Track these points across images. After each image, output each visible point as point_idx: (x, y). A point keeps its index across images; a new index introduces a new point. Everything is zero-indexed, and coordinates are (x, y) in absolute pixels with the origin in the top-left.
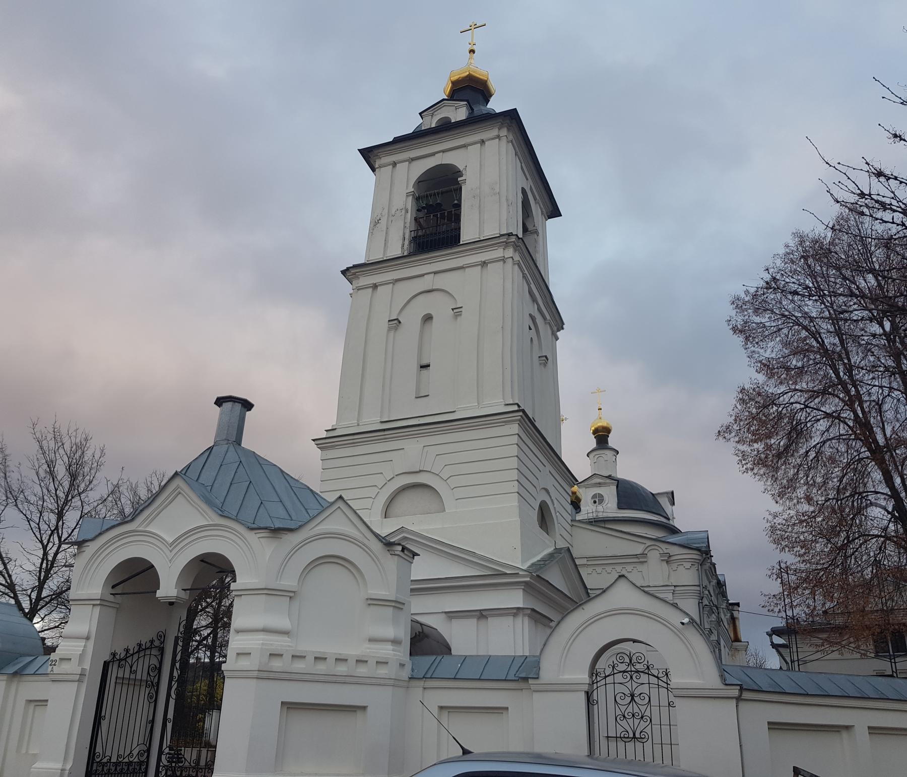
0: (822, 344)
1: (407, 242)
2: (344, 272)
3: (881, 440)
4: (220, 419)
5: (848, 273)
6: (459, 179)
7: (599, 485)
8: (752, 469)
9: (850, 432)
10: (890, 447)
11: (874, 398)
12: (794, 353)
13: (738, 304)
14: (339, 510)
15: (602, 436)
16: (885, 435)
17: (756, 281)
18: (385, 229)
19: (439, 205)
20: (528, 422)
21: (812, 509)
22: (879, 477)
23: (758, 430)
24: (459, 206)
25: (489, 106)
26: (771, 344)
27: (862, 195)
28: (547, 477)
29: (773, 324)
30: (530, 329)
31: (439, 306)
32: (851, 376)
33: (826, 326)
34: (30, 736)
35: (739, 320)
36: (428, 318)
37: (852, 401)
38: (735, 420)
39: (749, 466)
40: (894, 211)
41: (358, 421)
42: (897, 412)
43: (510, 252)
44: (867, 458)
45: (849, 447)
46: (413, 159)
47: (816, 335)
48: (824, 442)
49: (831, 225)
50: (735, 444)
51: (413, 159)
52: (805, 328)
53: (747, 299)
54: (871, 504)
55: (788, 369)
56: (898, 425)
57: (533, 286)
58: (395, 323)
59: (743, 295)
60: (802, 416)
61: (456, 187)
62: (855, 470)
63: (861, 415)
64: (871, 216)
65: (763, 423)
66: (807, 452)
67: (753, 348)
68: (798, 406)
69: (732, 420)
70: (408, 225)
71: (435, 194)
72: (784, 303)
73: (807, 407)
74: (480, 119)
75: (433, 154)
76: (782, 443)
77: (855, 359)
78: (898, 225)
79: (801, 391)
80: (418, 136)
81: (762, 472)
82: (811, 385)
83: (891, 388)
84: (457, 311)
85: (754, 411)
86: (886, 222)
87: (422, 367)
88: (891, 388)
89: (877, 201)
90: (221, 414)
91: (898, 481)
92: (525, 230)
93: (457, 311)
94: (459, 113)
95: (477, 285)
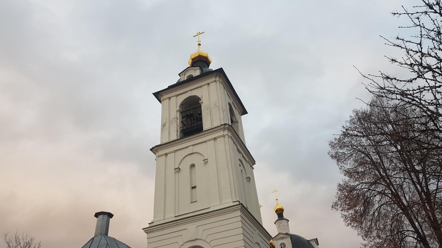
0: (372, 159)
1: (179, 133)
2: (151, 150)
3: (405, 203)
4: (97, 224)
5: (380, 126)
7: (282, 238)
8: (351, 224)
9: (391, 200)
10: (410, 206)
11: (398, 183)
12: (360, 165)
13: (332, 145)
15: (280, 213)
16: (406, 200)
17: (338, 132)
18: (168, 128)
19: (192, 114)
20: (244, 210)
21: (381, 241)
22: (408, 223)
23: (350, 203)
24: (201, 114)
25: (209, 68)
26: (349, 161)
27: (382, 88)
28: (257, 237)
29: (349, 152)
30: (240, 166)
31: (197, 160)
32: (386, 173)
33: (371, 151)
34: (175, 192)
35: (333, 152)
36: (193, 166)
37: (389, 185)
38: (339, 199)
39: (349, 222)
40: (397, 94)
41: (164, 217)
42: (409, 188)
43: (226, 132)
44: (401, 213)
45: (392, 208)
46: (178, 95)
47: (368, 155)
48: (380, 206)
49: (369, 104)
50: (340, 211)
51: (178, 95)
52: (363, 153)
53: (336, 142)
54: (407, 236)
55: (358, 173)
56: (411, 195)
57: (238, 146)
58: (178, 170)
59: (334, 141)
60: (368, 194)
61: (199, 105)
62: (397, 220)
63: (394, 191)
64: (387, 97)
65: (351, 200)
66: (374, 213)
67: (341, 165)
68: (365, 190)
69: (337, 199)
70: (178, 125)
71: (189, 110)
72: (353, 142)
73: (369, 190)
74: (206, 74)
76: (362, 209)
77: (386, 165)
78: (399, 100)
79: (365, 183)
80: (179, 84)
81: (355, 225)
82: (369, 180)
83: (405, 178)
84: (206, 161)
85: (346, 194)
86: (394, 99)
87: (192, 188)
88: (405, 178)
89: (388, 91)
90: (98, 221)
91: (417, 224)
92: (232, 121)
93: (206, 161)
94: (196, 72)
95: (213, 149)
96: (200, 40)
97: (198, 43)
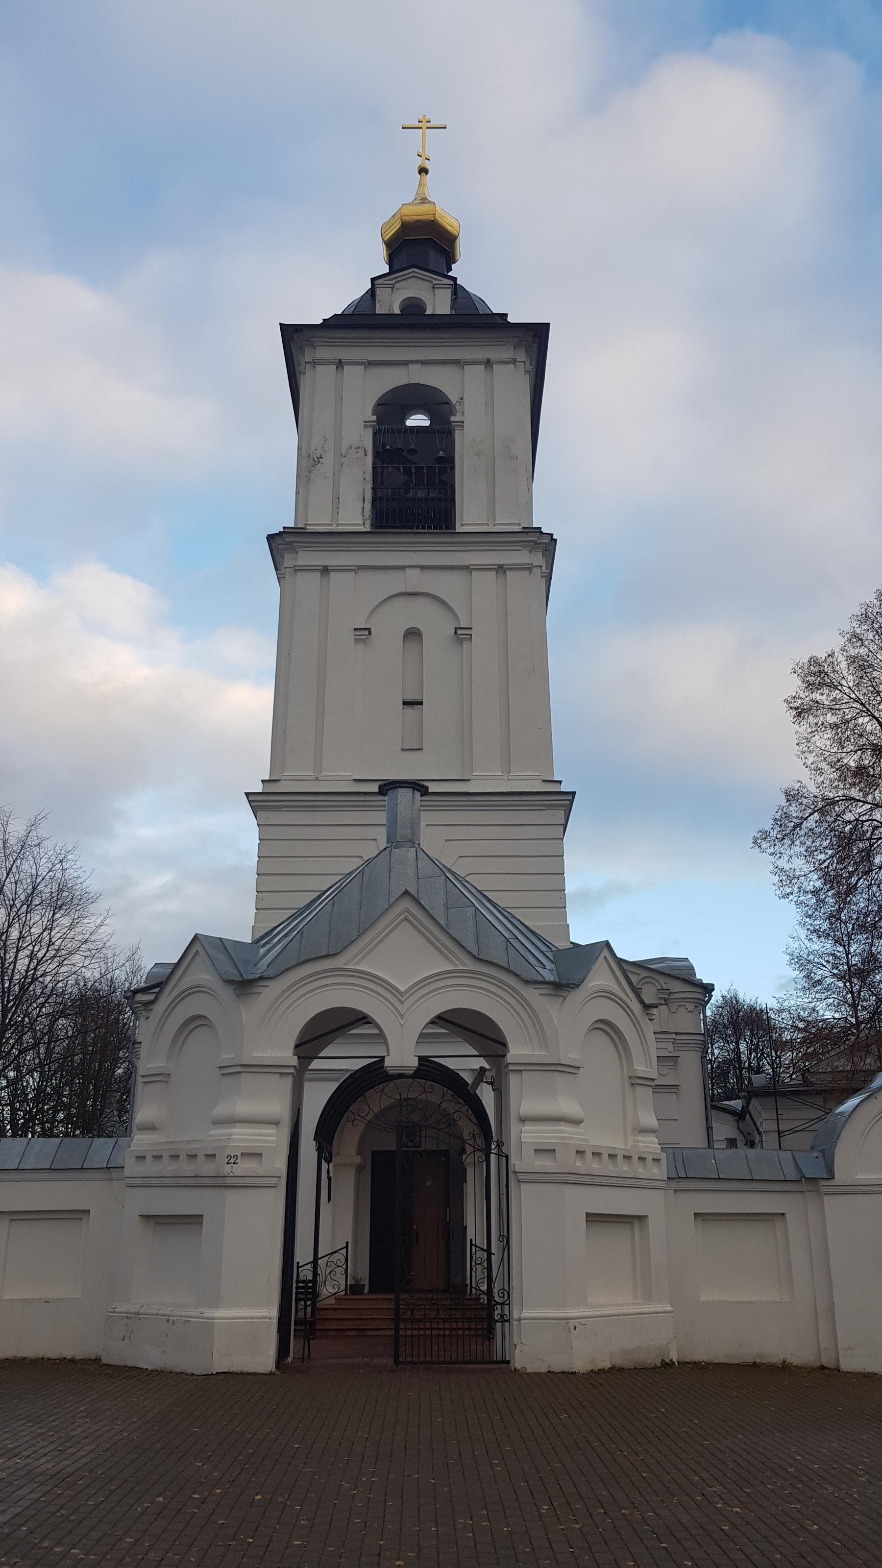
6: (452, 419)
14: (405, 922)
24: (450, 460)
58: (364, 633)
71: (393, 432)
75: (405, 363)
84: (462, 635)
93: (462, 635)
96: (427, 154)
97: (419, 162)
